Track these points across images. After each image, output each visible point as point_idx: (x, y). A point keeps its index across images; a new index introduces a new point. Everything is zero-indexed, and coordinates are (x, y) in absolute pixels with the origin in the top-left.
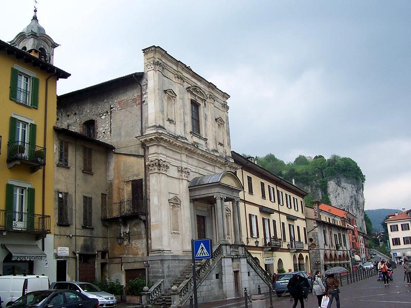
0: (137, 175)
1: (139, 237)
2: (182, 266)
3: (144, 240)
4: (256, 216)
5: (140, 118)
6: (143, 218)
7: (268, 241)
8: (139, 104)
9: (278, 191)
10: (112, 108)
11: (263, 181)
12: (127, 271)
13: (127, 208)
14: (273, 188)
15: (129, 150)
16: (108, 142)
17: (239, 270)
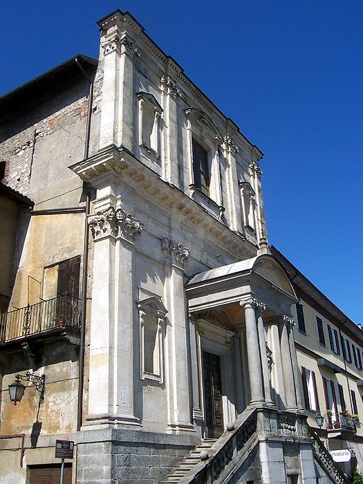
0: (70, 250)
1: (63, 384)
2: (165, 460)
3: (75, 394)
4: (313, 373)
5: (84, 139)
6: (73, 340)
7: (334, 418)
8: (84, 116)
9: (341, 337)
10: (37, 134)
11: (321, 317)
12: (30, 467)
13: (44, 322)
14: (335, 332)
15: (60, 203)
16: (22, 191)
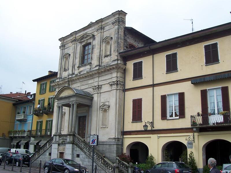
17: (64, 152)
